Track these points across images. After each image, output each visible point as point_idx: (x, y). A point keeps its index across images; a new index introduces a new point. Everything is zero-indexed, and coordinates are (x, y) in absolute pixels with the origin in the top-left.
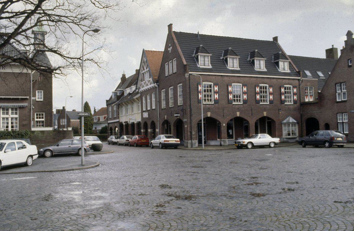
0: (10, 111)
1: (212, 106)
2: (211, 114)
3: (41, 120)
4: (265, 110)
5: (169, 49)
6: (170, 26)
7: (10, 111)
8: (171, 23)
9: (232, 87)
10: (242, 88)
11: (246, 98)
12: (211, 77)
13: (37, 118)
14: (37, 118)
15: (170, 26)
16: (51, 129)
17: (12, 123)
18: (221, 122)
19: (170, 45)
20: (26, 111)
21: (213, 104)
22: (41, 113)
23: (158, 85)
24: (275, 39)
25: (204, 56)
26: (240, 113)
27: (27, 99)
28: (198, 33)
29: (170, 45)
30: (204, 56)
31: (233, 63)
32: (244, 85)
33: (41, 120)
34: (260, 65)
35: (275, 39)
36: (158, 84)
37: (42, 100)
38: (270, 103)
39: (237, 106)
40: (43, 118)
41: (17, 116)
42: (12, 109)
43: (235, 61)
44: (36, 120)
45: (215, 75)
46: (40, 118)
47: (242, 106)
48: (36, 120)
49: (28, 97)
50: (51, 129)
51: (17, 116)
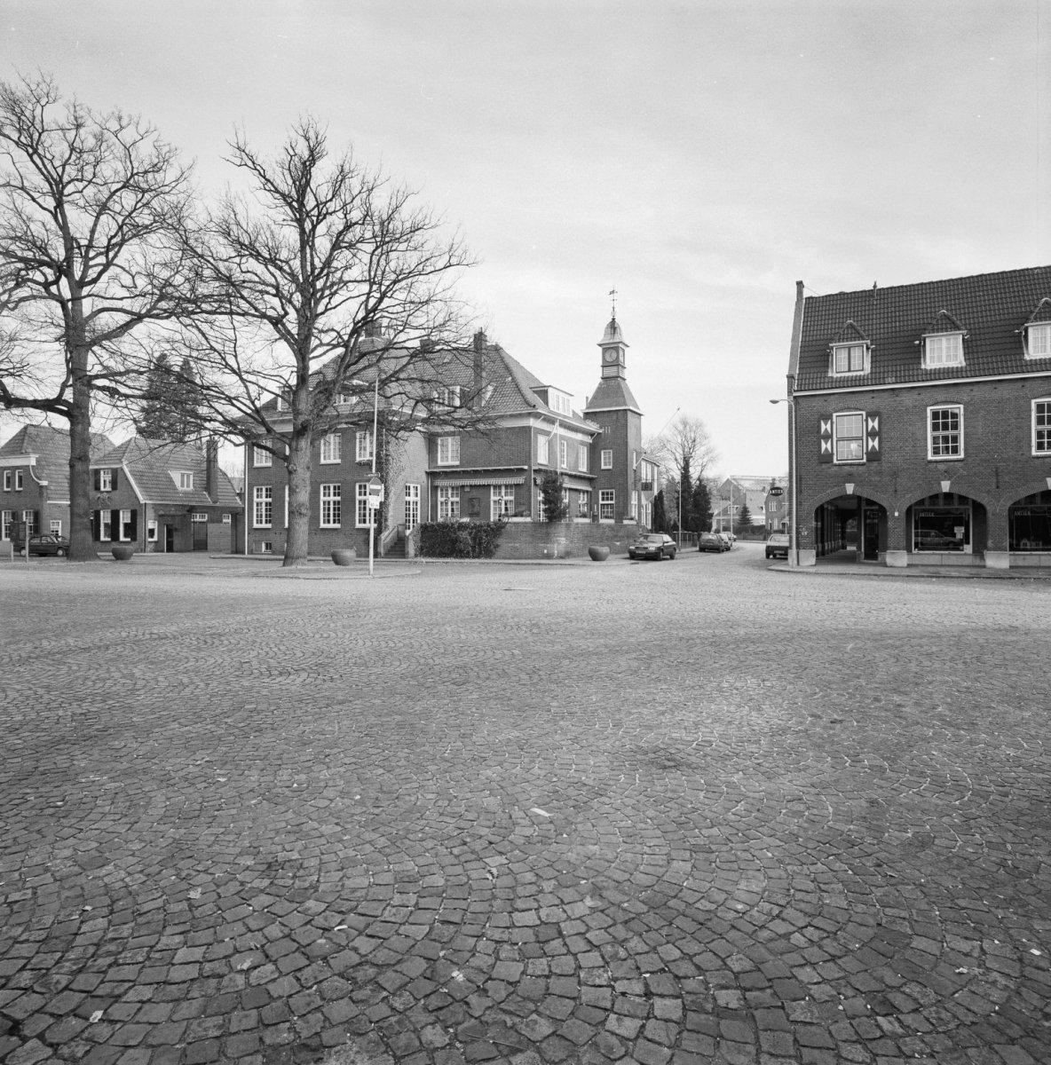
0: (503, 491)
1: (860, 468)
2: (855, 488)
3: (610, 502)
4: (849, 478)
6: (800, 284)
7: (503, 491)
8: (477, 331)
9: (832, 423)
10: (867, 420)
11: (877, 447)
12: (859, 397)
13: (603, 499)
14: (603, 499)
15: (800, 284)
16: (528, 519)
17: (453, 510)
18: (887, 508)
20: (523, 491)
21: (863, 464)
22: (609, 491)
25: (849, 348)
26: (951, 484)
27: (523, 470)
28: (875, 286)
30: (849, 348)
31: (944, 352)
32: (871, 415)
33: (610, 502)
34: (944, 352)
37: (611, 467)
38: (868, 460)
39: (941, 467)
40: (612, 499)
41: (512, 498)
42: (453, 488)
43: (856, 353)
44: (601, 502)
45: (873, 391)
46: (607, 499)
47: (960, 464)
48: (601, 502)
49: (526, 467)
50: (528, 519)
51: (458, 499)
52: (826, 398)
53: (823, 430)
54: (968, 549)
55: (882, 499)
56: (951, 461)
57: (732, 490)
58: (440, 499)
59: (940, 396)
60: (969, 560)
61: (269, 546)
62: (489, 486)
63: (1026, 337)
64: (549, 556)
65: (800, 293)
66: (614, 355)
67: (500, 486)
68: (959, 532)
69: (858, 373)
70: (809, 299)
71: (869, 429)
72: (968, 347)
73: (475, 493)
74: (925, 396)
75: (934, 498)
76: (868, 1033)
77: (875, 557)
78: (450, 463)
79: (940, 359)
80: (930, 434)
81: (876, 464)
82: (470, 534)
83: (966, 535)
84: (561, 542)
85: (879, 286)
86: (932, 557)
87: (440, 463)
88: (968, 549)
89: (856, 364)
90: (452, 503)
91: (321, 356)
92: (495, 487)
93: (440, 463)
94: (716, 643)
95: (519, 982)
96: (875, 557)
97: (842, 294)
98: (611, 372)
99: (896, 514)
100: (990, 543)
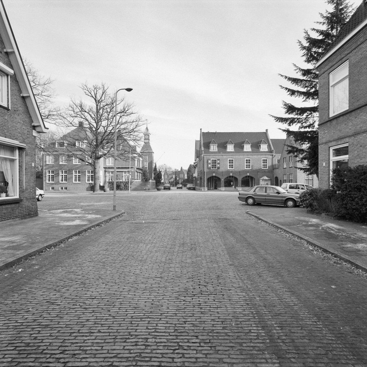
0: (127, 173)
4: (214, 172)
7: (110, 173)
15: (201, 129)
22: (247, 169)
39: (230, 170)
42: (111, 172)
54: (233, 187)
58: (107, 175)
59: (230, 156)
60: (234, 189)
61: (53, 188)
62: (123, 172)
63: (244, 146)
64: (145, 190)
65: (201, 131)
66: (148, 137)
67: (126, 172)
68: (232, 183)
70: (203, 132)
72: (218, 147)
73: (118, 173)
75: (246, 177)
77: (217, 189)
78: (110, 165)
79: (230, 149)
80: (228, 164)
82: (123, 184)
83: (233, 184)
84: (149, 186)
86: (228, 188)
87: (107, 165)
88: (233, 187)
89: (215, 148)
90: (111, 176)
92: (124, 172)
93: (107, 165)
94: (83, 225)
96: (217, 189)
97: (208, 132)
98: (147, 141)
100: (238, 186)
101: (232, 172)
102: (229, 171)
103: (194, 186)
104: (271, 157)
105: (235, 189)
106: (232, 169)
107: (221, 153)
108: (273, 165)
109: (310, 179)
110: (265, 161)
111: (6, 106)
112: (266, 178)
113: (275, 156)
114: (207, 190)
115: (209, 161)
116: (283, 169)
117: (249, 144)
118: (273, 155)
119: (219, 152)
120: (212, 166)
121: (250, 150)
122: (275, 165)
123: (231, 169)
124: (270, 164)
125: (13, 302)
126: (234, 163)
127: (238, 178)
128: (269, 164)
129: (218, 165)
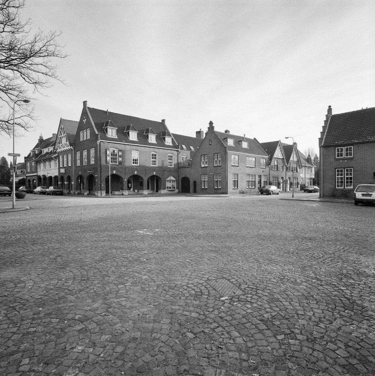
5: (84, 121)
6: (85, 103)
15: (85, 103)
19: (85, 118)
23: (74, 148)
24: (163, 121)
28: (107, 110)
29: (85, 118)
35: (163, 121)
36: (74, 147)
39: (135, 167)
52: (131, 146)
53: (121, 153)
55: (122, 175)
56: (137, 166)
57: (2, 164)
60: (132, 193)
69: (114, 137)
71: (119, 155)
74: (168, 151)
76: (268, 334)
81: (120, 165)
83: (131, 186)
85: (109, 111)
91: (37, 57)
95: (10, 347)
99: (125, 180)
100: (144, 188)
101: (136, 169)
102: (134, 168)
103: (61, 190)
104: (176, 153)
105: (134, 193)
106: (136, 165)
107: (123, 141)
108: (178, 164)
109: (250, 181)
110: (171, 158)
111: (25, 62)
112: (173, 178)
113: (180, 152)
114: (105, 194)
115: (108, 152)
116: (200, 169)
117: (136, 130)
118: (178, 151)
119: (119, 140)
120: (112, 158)
121: (135, 139)
122: (181, 163)
123: (135, 165)
124: (176, 162)
125: (130, 294)
126: (173, 160)
127: (143, 177)
128: (174, 161)
129: (120, 159)
